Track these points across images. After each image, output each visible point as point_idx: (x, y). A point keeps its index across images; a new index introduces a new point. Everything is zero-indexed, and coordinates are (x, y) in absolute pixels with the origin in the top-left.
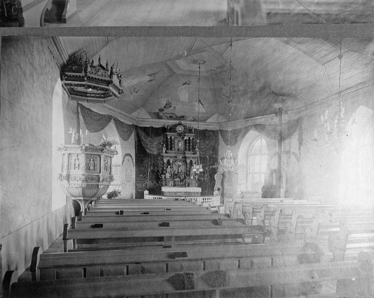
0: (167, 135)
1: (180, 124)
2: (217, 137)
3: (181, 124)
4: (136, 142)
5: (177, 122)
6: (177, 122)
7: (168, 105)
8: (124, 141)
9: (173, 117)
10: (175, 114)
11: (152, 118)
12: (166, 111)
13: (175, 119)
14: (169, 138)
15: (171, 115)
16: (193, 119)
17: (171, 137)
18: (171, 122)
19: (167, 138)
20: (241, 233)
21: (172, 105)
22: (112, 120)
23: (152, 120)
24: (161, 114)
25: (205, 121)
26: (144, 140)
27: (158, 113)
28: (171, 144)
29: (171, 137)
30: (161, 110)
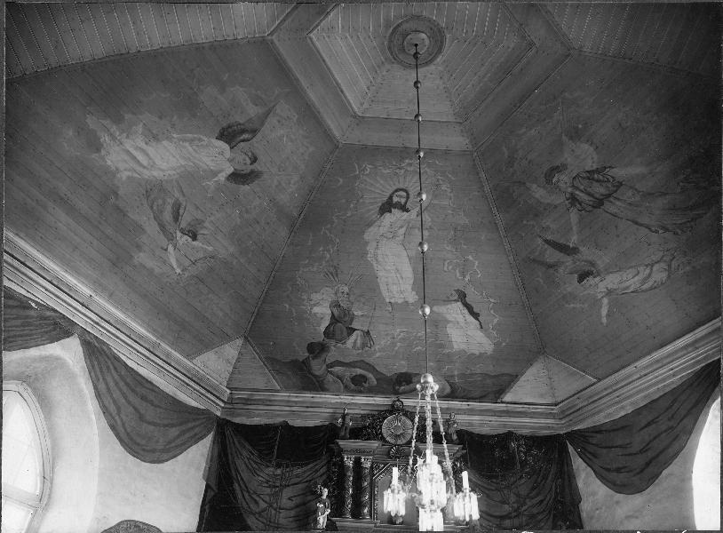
0: (341, 451)
1: (393, 410)
2: (564, 460)
3: (398, 410)
4: (208, 487)
5: (381, 401)
6: (381, 401)
7: (341, 323)
8: (167, 466)
9: (364, 378)
10: (371, 368)
11: (287, 388)
12: (333, 354)
13: (372, 391)
14: (350, 463)
15: (359, 371)
16: (448, 390)
17: (357, 462)
18: (363, 403)
19: (342, 465)
20: (449, 317)
21: (354, 325)
22: (28, 63)
23: (283, 395)
24: (318, 367)
25: (497, 394)
26: (245, 475)
27: (305, 363)
28: (359, 490)
29: (357, 462)
30: (317, 349)
